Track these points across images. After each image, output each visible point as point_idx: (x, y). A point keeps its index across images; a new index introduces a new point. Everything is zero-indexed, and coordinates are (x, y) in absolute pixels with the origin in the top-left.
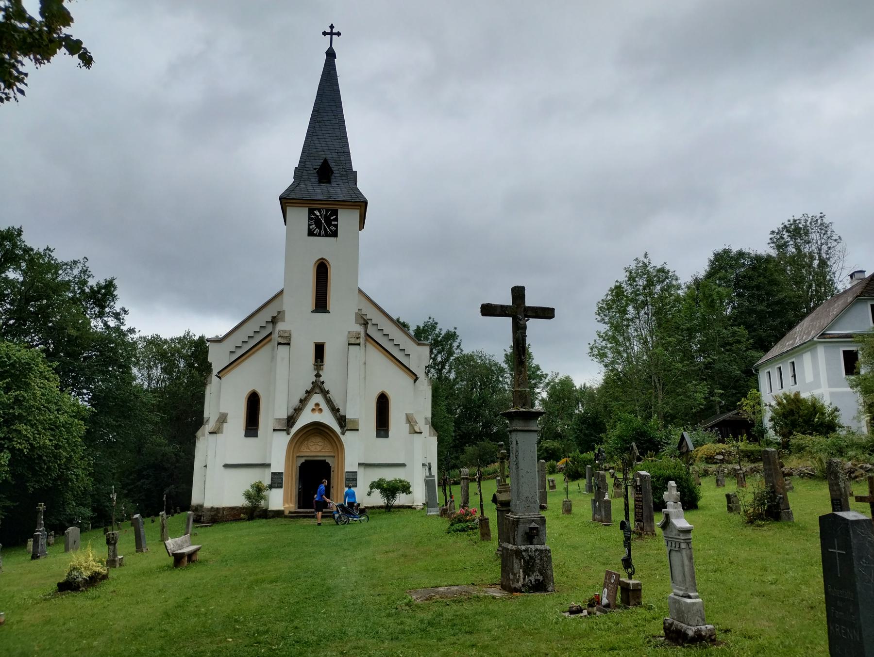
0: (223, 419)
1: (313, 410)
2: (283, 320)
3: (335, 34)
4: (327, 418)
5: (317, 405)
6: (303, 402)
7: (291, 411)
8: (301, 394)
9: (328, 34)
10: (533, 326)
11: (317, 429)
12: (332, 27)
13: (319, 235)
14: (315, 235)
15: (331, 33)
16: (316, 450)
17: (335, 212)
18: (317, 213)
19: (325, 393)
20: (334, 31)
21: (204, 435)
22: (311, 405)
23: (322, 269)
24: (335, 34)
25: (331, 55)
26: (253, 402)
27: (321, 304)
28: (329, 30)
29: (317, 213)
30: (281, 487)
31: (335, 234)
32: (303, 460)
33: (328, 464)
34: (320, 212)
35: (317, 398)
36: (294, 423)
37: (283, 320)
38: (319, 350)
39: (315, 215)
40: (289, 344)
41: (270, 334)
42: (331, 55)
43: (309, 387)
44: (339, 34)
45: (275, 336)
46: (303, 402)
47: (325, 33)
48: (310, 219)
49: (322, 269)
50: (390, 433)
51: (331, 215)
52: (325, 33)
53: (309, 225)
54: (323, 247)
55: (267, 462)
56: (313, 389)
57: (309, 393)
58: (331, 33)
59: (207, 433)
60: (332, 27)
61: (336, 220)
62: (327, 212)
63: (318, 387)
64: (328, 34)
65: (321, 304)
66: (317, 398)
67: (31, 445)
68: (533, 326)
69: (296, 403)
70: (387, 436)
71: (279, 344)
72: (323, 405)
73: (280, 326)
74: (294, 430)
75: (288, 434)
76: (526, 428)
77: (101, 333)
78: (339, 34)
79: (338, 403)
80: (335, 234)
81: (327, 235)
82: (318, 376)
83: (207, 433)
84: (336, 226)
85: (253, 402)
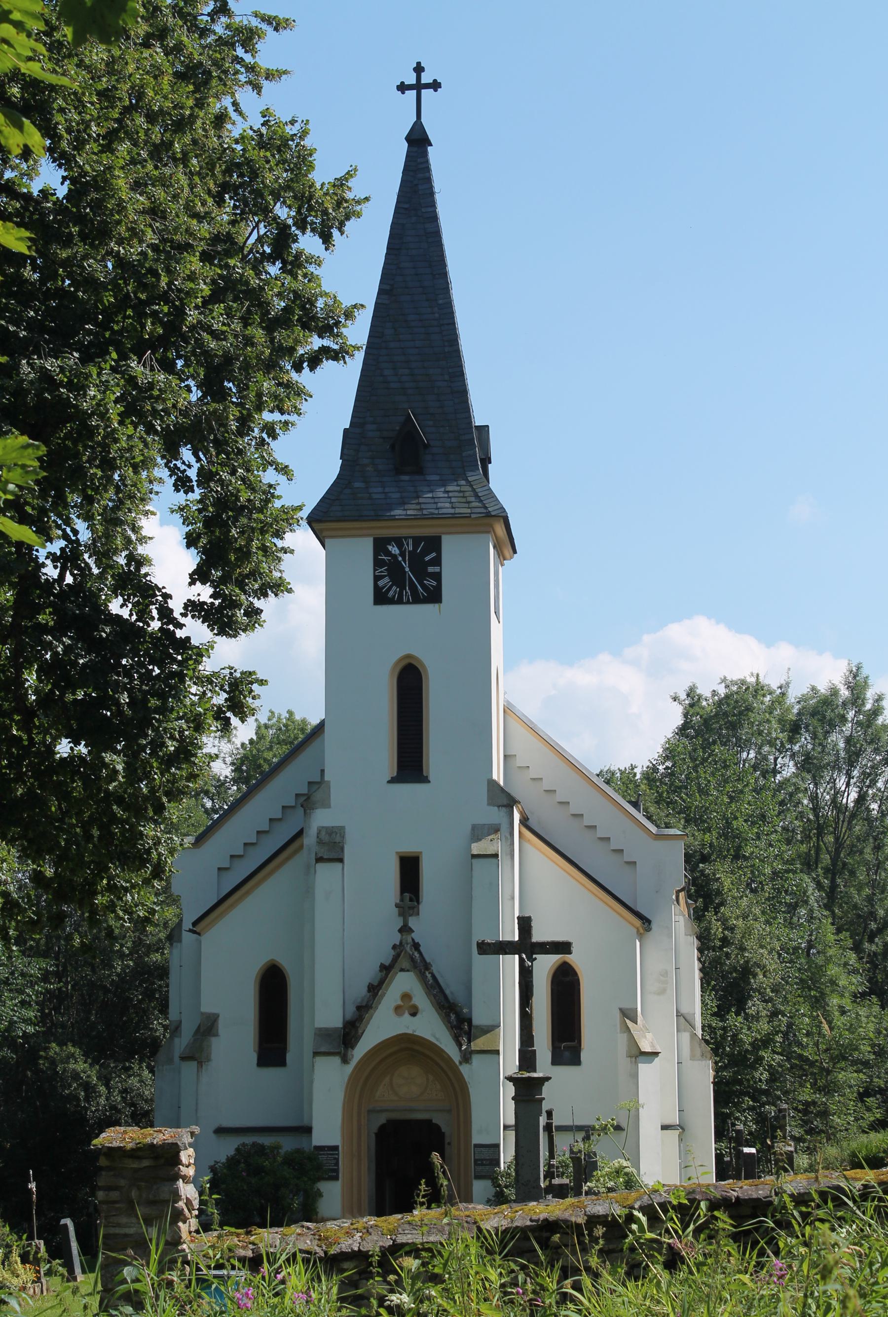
0: (208, 1027)
1: (398, 1010)
2: (326, 804)
3: (427, 86)
4: (430, 1026)
5: (406, 997)
6: (375, 990)
7: (351, 1009)
8: (369, 973)
9: (410, 87)
10: (538, 936)
11: (407, 1049)
12: (419, 69)
13: (400, 601)
14: (391, 601)
15: (419, 85)
16: (408, 1094)
17: (434, 544)
18: (395, 550)
19: (421, 967)
20: (426, 79)
21: (170, 1061)
22: (391, 996)
23: (410, 683)
24: (427, 86)
25: (418, 140)
26: (273, 988)
27: (410, 764)
28: (411, 79)
29: (395, 550)
30: (336, 1178)
31: (434, 596)
32: (382, 1119)
33: (438, 1128)
34: (400, 546)
35: (405, 982)
36: (357, 1038)
37: (326, 804)
38: (410, 869)
39: (389, 553)
40: (341, 860)
41: (300, 833)
42: (418, 140)
43: (386, 956)
44: (435, 85)
45: (310, 839)
46: (375, 990)
47: (403, 88)
48: (377, 563)
49: (410, 683)
50: (583, 1056)
51: (426, 552)
52: (403, 88)
53: (377, 579)
54: (408, 628)
55: (305, 1123)
56: (396, 959)
57: (386, 970)
58: (419, 85)
59: (176, 1059)
60: (419, 69)
61: (437, 561)
62: (415, 546)
63: (407, 955)
64: (410, 87)
65: (410, 764)
66: (405, 982)
67: (193, 118)
68: (538, 936)
69: (360, 991)
70: (576, 1061)
71: (319, 860)
72: (421, 999)
73: (321, 819)
74: (360, 1051)
75: (345, 1060)
76: (249, 1140)
77: (28, 699)
78: (435, 85)
79: (452, 988)
80: (434, 596)
81: (417, 600)
82: (405, 929)
83: (176, 1059)
84: (438, 577)
85: (273, 988)
